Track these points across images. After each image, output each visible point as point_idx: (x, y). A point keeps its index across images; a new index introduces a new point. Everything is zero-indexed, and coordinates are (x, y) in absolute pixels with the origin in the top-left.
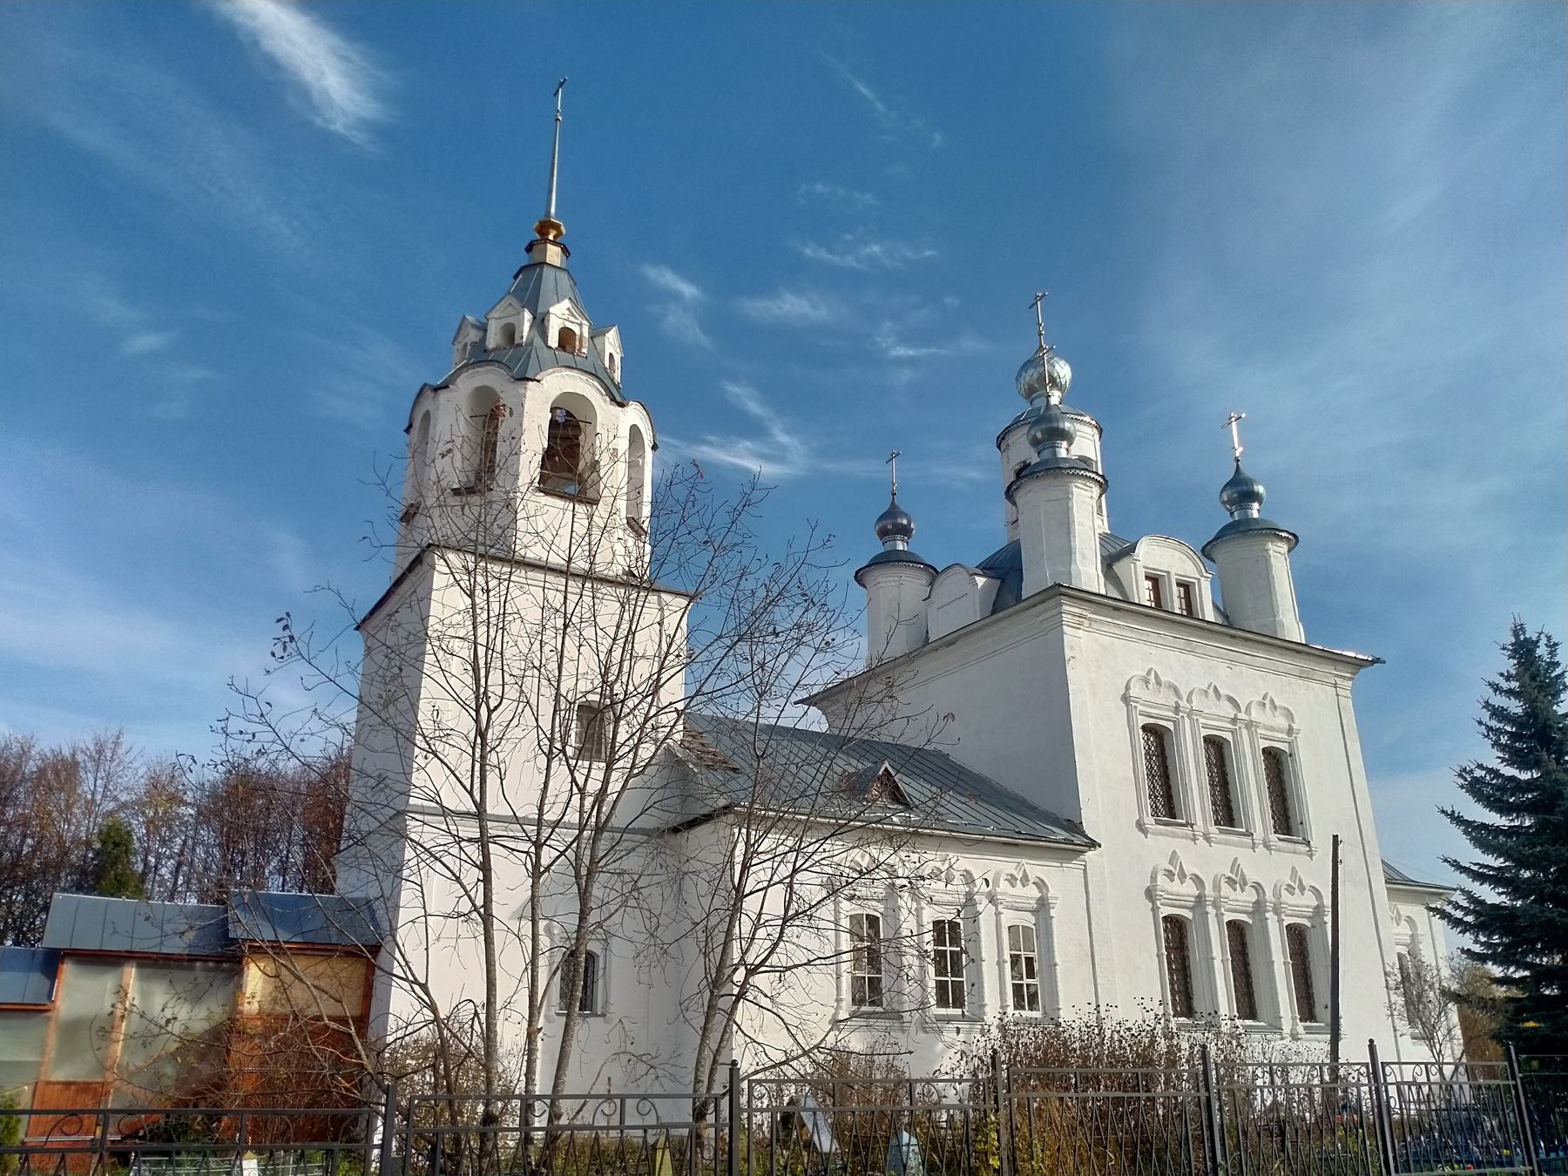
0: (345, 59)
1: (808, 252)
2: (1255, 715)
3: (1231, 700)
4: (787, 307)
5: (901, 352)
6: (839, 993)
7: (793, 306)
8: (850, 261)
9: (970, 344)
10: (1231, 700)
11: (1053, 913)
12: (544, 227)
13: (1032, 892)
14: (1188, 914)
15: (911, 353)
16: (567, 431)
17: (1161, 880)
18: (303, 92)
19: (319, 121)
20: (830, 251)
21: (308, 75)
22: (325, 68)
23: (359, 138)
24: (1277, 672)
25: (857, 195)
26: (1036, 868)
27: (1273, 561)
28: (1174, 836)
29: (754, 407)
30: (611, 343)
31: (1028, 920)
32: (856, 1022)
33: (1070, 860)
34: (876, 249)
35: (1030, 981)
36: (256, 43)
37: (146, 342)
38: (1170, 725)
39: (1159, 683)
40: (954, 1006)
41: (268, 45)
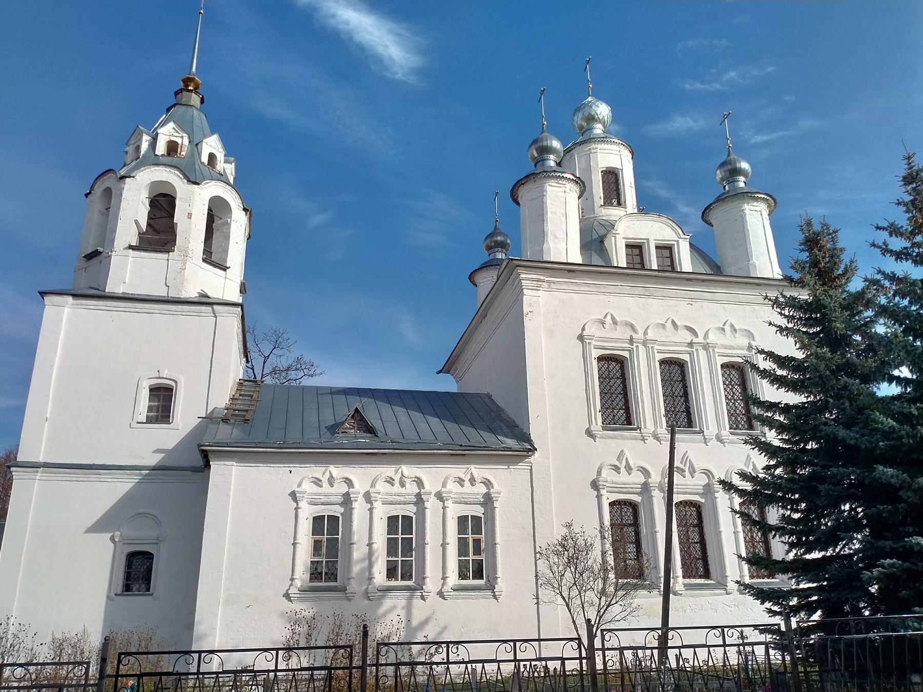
0: (398, 35)
1: (687, 86)
2: (712, 338)
3: (689, 329)
4: (678, 125)
5: (759, 138)
6: (444, 572)
7: (682, 123)
8: (717, 86)
9: (806, 123)
10: (689, 329)
11: (496, 504)
12: (187, 81)
13: (412, 488)
14: (637, 498)
15: (766, 138)
16: (163, 204)
17: (607, 474)
18: (378, 59)
19: (389, 75)
20: (702, 83)
21: (380, 50)
22: (389, 44)
23: (412, 79)
24: (741, 303)
25: (715, 42)
26: (479, 471)
27: (748, 218)
28: (623, 438)
29: (663, 193)
30: (212, 145)
31: (479, 511)
32: (621, 593)
33: (516, 463)
34: (733, 74)
35: (476, 557)
36: (351, 39)
37: (318, 219)
38: (626, 354)
39: (615, 322)
40: (403, 578)
41: (358, 38)
